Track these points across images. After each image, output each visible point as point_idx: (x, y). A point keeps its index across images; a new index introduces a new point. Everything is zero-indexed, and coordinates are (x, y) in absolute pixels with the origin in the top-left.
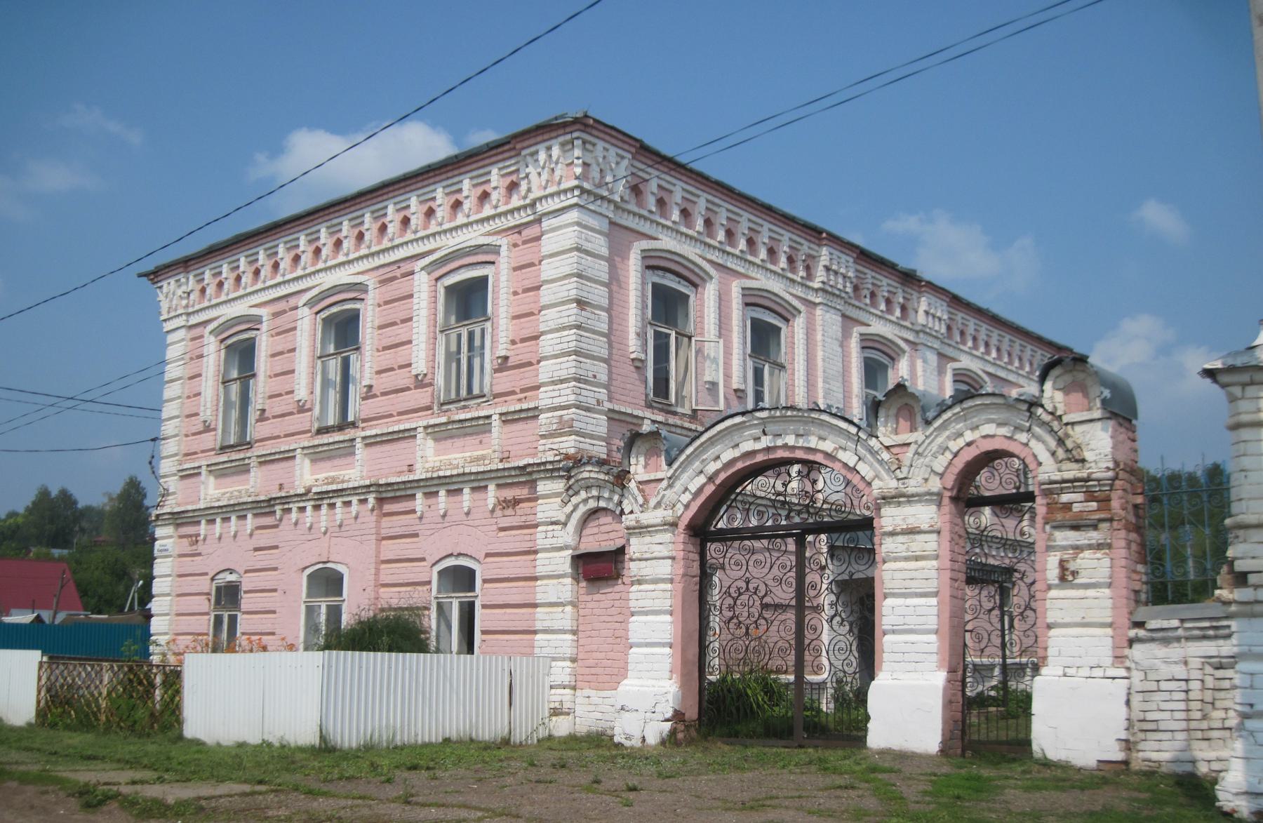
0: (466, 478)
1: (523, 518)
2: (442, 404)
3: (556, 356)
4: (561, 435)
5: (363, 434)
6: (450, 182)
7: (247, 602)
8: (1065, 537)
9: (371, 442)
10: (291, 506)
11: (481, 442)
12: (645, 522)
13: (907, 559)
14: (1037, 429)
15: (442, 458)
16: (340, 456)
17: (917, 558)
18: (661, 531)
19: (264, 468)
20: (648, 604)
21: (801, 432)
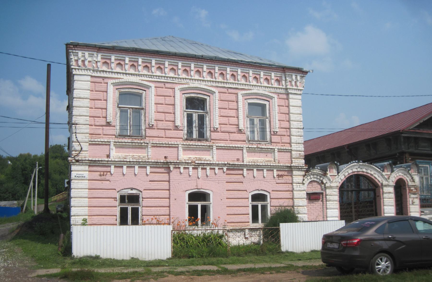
1: (286, 181)
2: (249, 141)
3: (296, 136)
4: (299, 159)
5: (217, 145)
7: (143, 202)
8: (413, 196)
9: (219, 148)
11: (266, 156)
13: (388, 198)
14: (408, 175)
15: (118, 154)
16: (199, 150)
17: (390, 198)
18: (335, 188)
19: (154, 148)
20: (332, 207)
21: (367, 169)
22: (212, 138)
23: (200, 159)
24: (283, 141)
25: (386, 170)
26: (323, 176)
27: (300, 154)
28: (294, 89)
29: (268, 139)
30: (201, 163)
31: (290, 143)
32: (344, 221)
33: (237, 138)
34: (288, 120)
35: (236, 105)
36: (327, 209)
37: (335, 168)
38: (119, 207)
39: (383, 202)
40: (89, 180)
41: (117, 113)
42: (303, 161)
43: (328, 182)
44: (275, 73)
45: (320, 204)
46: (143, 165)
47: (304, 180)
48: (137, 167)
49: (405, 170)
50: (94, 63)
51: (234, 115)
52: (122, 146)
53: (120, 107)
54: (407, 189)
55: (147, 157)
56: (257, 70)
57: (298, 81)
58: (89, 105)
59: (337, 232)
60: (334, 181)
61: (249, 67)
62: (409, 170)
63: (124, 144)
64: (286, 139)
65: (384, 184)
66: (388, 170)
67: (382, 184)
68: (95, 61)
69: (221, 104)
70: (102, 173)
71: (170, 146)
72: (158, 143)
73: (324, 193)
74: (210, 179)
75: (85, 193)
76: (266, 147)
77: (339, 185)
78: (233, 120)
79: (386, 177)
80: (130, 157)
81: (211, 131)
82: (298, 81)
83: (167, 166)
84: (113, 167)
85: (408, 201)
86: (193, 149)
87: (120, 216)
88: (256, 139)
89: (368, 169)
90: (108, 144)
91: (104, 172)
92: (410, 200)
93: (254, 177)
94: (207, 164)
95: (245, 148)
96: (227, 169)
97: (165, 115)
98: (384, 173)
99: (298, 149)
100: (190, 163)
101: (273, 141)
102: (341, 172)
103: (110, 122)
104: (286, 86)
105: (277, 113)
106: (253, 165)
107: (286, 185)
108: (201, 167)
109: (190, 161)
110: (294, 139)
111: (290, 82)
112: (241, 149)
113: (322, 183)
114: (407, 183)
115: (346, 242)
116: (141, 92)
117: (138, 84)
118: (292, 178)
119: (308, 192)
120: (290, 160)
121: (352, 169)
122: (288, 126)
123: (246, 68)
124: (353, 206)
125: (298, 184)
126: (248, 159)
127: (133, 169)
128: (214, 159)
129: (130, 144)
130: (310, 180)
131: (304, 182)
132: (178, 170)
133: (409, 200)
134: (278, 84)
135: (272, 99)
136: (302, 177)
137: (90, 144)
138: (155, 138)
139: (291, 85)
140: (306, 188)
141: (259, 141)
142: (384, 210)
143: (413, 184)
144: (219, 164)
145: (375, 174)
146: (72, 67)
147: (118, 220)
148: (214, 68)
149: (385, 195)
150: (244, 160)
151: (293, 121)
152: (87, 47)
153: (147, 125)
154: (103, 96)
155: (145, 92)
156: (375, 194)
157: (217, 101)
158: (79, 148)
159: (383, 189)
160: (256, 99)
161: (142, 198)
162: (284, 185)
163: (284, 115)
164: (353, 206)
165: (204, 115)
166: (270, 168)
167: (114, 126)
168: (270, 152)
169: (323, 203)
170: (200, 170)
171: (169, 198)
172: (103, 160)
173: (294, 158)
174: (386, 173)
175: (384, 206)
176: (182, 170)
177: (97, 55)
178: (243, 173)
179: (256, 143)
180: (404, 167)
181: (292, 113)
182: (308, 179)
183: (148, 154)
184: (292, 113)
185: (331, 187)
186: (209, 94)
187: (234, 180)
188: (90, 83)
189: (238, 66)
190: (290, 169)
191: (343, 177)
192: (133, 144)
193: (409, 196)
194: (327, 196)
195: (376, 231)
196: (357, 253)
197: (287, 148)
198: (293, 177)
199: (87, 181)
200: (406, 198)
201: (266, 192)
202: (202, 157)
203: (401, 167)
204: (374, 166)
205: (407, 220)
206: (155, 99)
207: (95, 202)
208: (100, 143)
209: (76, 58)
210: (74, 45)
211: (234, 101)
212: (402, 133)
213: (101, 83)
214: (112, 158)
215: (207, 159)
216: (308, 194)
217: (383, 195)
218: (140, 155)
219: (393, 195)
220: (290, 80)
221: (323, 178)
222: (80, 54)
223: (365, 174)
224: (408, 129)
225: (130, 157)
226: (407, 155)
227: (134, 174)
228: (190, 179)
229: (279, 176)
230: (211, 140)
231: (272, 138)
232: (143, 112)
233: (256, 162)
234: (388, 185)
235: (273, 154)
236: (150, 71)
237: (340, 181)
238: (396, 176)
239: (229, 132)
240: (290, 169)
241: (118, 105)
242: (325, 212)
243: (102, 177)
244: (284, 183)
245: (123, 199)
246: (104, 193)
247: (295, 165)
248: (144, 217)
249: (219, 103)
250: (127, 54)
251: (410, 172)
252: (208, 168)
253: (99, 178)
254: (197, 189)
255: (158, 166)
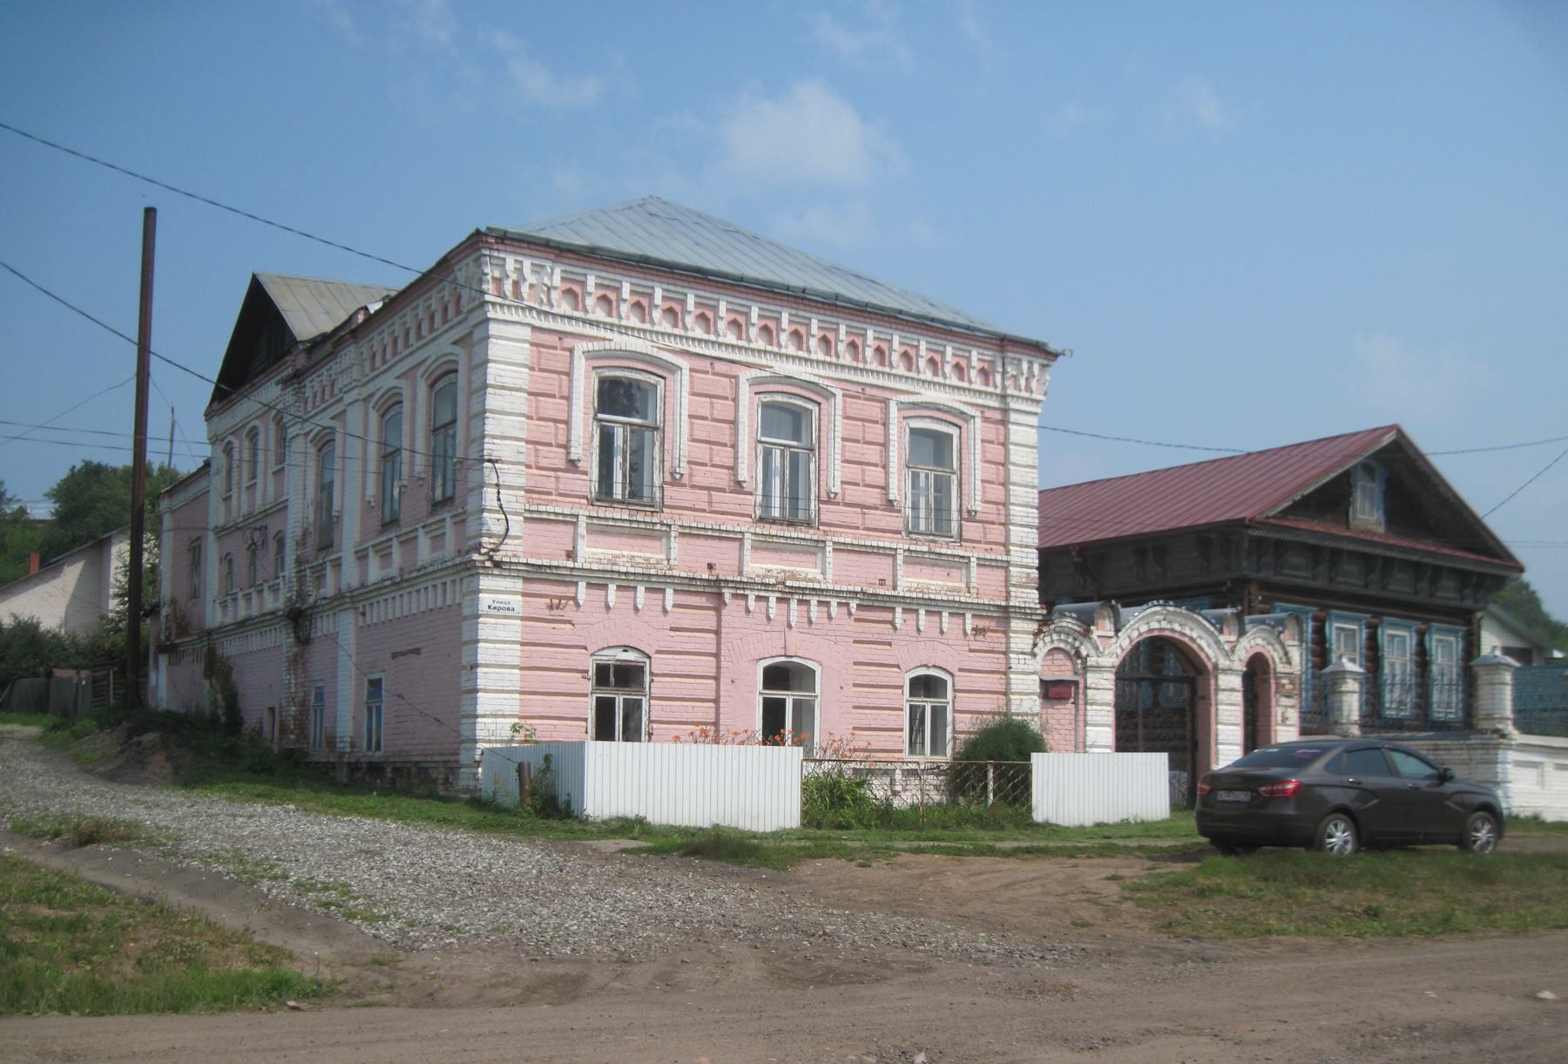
0: (969, 606)
1: (992, 645)
2: (910, 533)
3: (1022, 526)
4: (1026, 588)
5: (835, 539)
6: (963, 347)
7: (658, 687)
8: (1284, 701)
9: (840, 548)
10: (747, 592)
12: (1101, 664)
13: (1227, 704)
14: (1277, 647)
15: (594, 550)
16: (791, 552)
19: (685, 540)
22: (824, 518)
23: (794, 576)
24: (990, 537)
25: (1225, 630)
26: (1081, 638)
27: (1028, 574)
28: (1023, 398)
29: (955, 531)
30: (799, 588)
31: (1006, 545)
32: (1163, 757)
33: (883, 525)
34: (1002, 481)
35: (883, 432)
36: (1086, 724)
37: (1109, 617)
38: (594, 696)
39: (1217, 715)
40: (523, 619)
41: (593, 436)
42: (1035, 595)
43: (1092, 652)
44: (981, 351)
45: (1068, 712)
46: (656, 583)
47: (1035, 645)
48: (643, 588)
49: (1271, 633)
50: (543, 292)
51: (876, 459)
52: (605, 529)
53: (600, 420)
54: (1273, 681)
55: (665, 563)
56: (939, 342)
57: (1034, 376)
58: (525, 410)
59: (1235, 769)
60: (1107, 652)
61: (919, 331)
62: (1280, 633)
63: (611, 523)
64: (996, 533)
65: (1220, 666)
66: (1232, 628)
67: (1216, 666)
68: (545, 285)
69: (848, 427)
70: (556, 601)
71: (721, 536)
72: (694, 525)
73: (1081, 681)
74: (816, 632)
75: (514, 654)
76: (949, 552)
77: (1116, 661)
78: (874, 473)
79: (1227, 647)
80: (625, 559)
81: (820, 501)
82: (1034, 376)
83: (714, 590)
84: (582, 585)
85: (1273, 713)
86: (777, 546)
87: (594, 721)
88: (922, 527)
89: (1185, 625)
90: (571, 521)
91: (560, 598)
92: (1277, 713)
93: (919, 630)
94: (814, 589)
95: (902, 552)
96: (858, 605)
97: (711, 449)
98: (1222, 638)
99: (1024, 560)
100: (774, 585)
101: (966, 535)
102: (1124, 630)
103: (579, 461)
104: (1004, 387)
105: (978, 461)
106: (919, 599)
107: (991, 655)
108: (796, 597)
109: (772, 581)
110: (1017, 534)
111: (1014, 377)
112: (891, 554)
113: (1078, 654)
114: (1272, 667)
115: (1270, 788)
116: (652, 381)
117: (648, 359)
118: (1008, 638)
119: (1044, 678)
120: (1004, 589)
121: (1148, 623)
122: (1001, 498)
123: (913, 333)
124: (1140, 720)
125: (1021, 656)
126: (910, 581)
127: (631, 594)
128: (827, 577)
129: (627, 524)
130: (1050, 647)
131: (1036, 650)
132: (742, 603)
133: (1276, 712)
134: (983, 380)
135: (967, 422)
136: (1032, 637)
137: (526, 519)
138: (686, 512)
139: (1017, 387)
140: (1039, 668)
141: (934, 535)
142: (1217, 735)
143: (1287, 670)
144: (840, 592)
145: (1201, 638)
146: (487, 298)
147: (589, 731)
148: (834, 327)
149: (1222, 696)
150: (899, 583)
151: (1015, 484)
152: (531, 247)
153: (667, 475)
154: (560, 386)
155: (662, 381)
156: (1194, 691)
157: (839, 418)
158: (498, 529)
159: (1216, 680)
160: (928, 420)
161: (652, 674)
162: (986, 655)
163: (994, 466)
164: (1140, 720)
165: (801, 456)
166: (958, 608)
167: (585, 473)
168: (958, 565)
169: (1077, 710)
170: (794, 605)
171: (717, 678)
172: (561, 565)
173: (1014, 585)
174: (1228, 637)
175: (1217, 723)
176: (752, 603)
177: (552, 270)
178: (576, 593)
179: (926, 541)
180: (1268, 624)
181: (1015, 464)
182: (1045, 644)
183: (668, 554)
184: (1015, 464)
185: (1098, 668)
186: (819, 399)
187: (870, 636)
188: (528, 346)
189: (893, 326)
190: (1005, 614)
191: (1127, 641)
192: (634, 525)
193: (1277, 701)
194: (1089, 692)
195: (1327, 767)
196: (1290, 811)
197: (999, 558)
198: (1011, 635)
199: (519, 622)
200: (1268, 707)
201: (939, 671)
202: (798, 569)
203: (1263, 622)
204: (1200, 618)
205: (1379, 748)
206: (690, 402)
207: (539, 680)
208: (552, 517)
209: (497, 274)
210: (496, 238)
211: (876, 422)
212: (1248, 527)
213: (555, 348)
214: (900, 592)
215: (809, 576)
216: (1044, 684)
217: (1216, 694)
218: (648, 555)
219: (1238, 697)
220: (1014, 373)
221: (1081, 644)
222: (510, 262)
223: (1177, 636)
224: (1264, 515)
225: (625, 559)
226: (1253, 589)
227: (632, 607)
228: (768, 628)
229: (977, 631)
230: (821, 523)
231: (964, 528)
232: (657, 435)
233: (926, 591)
234: (1230, 670)
235: (964, 572)
236: (680, 324)
237: (1119, 651)
238: (1248, 646)
239: (862, 506)
240: (1005, 614)
241: (596, 415)
242: (1081, 734)
243: (555, 612)
244: (988, 652)
245: (603, 674)
246: (559, 656)
247: (1017, 605)
248: (655, 726)
249: (843, 424)
250: (625, 272)
251: (1282, 636)
252: (814, 600)
253: (546, 614)
254: (786, 656)
255: (693, 589)
